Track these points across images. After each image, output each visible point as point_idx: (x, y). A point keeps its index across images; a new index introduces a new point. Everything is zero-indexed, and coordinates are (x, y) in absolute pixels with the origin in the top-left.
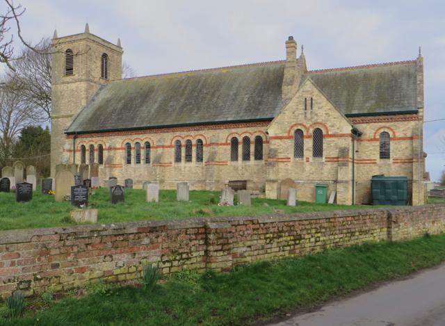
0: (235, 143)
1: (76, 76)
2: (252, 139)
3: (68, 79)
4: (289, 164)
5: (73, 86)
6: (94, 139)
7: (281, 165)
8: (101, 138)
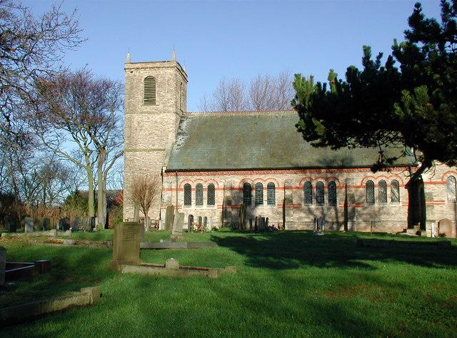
0: (188, 189)
1: (161, 106)
2: (205, 186)
3: (149, 108)
4: (444, 207)
5: (157, 117)
6: (202, 177)
7: (437, 207)
8: (212, 177)
